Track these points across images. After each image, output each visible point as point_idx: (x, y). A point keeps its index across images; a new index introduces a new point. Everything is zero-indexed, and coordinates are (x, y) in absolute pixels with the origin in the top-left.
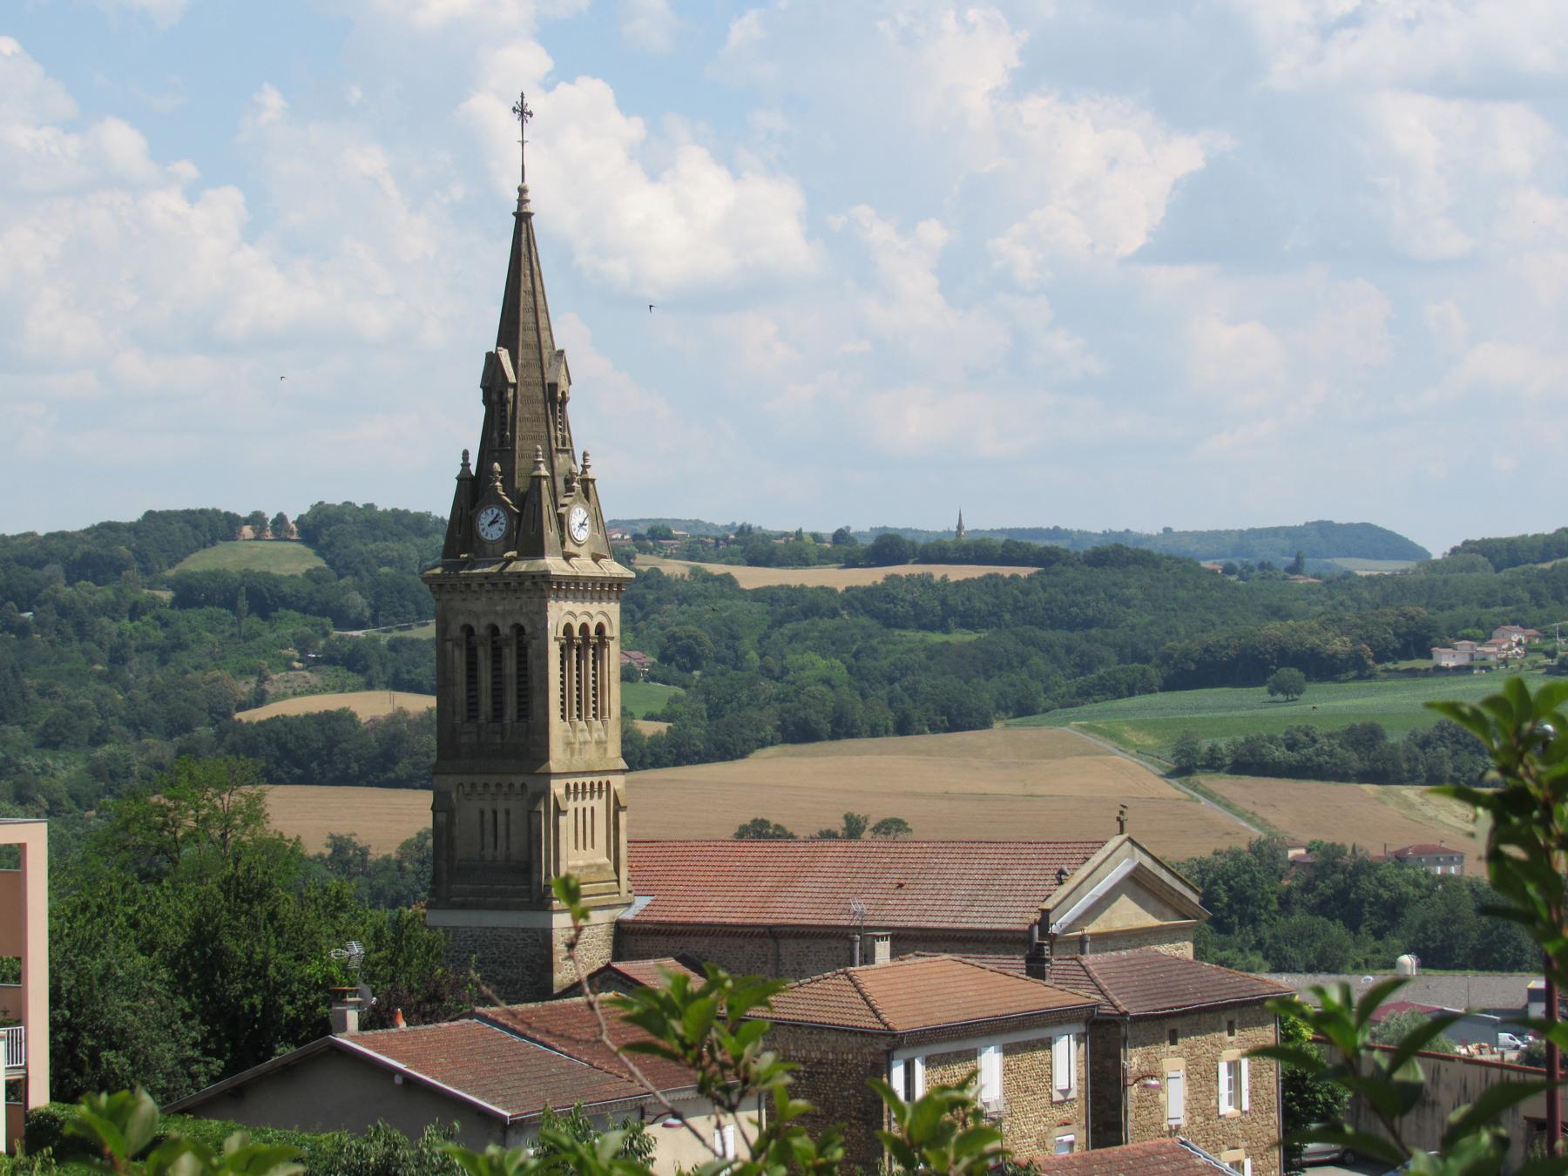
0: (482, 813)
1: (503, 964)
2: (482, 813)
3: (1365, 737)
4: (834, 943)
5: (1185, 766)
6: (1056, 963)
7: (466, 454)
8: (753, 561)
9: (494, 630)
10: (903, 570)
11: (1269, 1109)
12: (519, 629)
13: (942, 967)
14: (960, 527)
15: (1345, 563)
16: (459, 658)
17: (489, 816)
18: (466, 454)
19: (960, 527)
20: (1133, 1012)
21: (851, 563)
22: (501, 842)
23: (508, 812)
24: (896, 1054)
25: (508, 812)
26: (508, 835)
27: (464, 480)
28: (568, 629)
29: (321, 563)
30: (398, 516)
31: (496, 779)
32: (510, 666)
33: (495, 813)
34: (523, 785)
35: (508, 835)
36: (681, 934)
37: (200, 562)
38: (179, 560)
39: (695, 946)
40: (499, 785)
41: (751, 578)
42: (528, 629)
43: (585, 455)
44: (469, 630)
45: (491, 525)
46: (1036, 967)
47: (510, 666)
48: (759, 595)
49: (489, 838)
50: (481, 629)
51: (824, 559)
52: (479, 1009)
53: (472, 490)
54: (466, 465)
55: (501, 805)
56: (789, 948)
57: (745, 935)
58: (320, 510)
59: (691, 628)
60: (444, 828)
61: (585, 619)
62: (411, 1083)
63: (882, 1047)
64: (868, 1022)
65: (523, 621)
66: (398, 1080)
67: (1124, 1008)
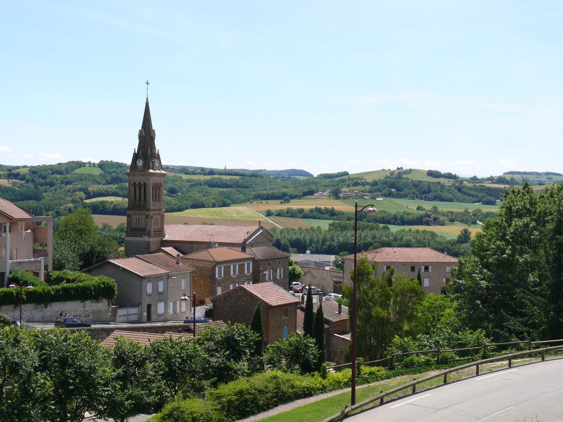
0: (136, 218)
1: (140, 248)
2: (136, 218)
3: (301, 211)
4: (204, 245)
5: (269, 214)
6: (248, 250)
7: (135, 149)
8: (186, 174)
9: (140, 183)
10: (214, 176)
11: (286, 278)
12: (145, 183)
13: (225, 249)
14: (225, 168)
15: (298, 177)
16: (133, 188)
17: (138, 219)
18: (135, 149)
19: (225, 168)
20: (262, 259)
21: (205, 174)
22: (140, 224)
23: (141, 218)
24: (217, 266)
25: (141, 218)
26: (141, 223)
27: (134, 154)
28: (154, 184)
29: (103, 172)
30: (117, 163)
31: (139, 212)
32: (142, 190)
33: (139, 219)
34: (145, 213)
35: (141, 223)
36: (175, 242)
37: (78, 171)
38: (74, 170)
39: (177, 245)
40: (137, 213)
41: (185, 177)
42: (146, 183)
43: (158, 150)
44: (135, 183)
45: (140, 163)
46: (244, 250)
47: (142, 190)
48: (188, 181)
49: (138, 223)
50: (137, 183)
51: (199, 174)
52: (137, 255)
53: (136, 157)
54: (135, 151)
55: (140, 217)
56: (195, 246)
57: (187, 243)
58: (102, 161)
59: (174, 186)
60: (129, 223)
61: (157, 181)
62: (124, 269)
63: (214, 264)
64: (212, 259)
65: (145, 182)
66: (121, 269)
67: (260, 258)
